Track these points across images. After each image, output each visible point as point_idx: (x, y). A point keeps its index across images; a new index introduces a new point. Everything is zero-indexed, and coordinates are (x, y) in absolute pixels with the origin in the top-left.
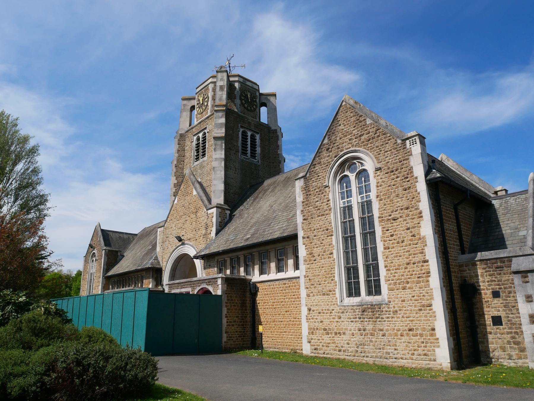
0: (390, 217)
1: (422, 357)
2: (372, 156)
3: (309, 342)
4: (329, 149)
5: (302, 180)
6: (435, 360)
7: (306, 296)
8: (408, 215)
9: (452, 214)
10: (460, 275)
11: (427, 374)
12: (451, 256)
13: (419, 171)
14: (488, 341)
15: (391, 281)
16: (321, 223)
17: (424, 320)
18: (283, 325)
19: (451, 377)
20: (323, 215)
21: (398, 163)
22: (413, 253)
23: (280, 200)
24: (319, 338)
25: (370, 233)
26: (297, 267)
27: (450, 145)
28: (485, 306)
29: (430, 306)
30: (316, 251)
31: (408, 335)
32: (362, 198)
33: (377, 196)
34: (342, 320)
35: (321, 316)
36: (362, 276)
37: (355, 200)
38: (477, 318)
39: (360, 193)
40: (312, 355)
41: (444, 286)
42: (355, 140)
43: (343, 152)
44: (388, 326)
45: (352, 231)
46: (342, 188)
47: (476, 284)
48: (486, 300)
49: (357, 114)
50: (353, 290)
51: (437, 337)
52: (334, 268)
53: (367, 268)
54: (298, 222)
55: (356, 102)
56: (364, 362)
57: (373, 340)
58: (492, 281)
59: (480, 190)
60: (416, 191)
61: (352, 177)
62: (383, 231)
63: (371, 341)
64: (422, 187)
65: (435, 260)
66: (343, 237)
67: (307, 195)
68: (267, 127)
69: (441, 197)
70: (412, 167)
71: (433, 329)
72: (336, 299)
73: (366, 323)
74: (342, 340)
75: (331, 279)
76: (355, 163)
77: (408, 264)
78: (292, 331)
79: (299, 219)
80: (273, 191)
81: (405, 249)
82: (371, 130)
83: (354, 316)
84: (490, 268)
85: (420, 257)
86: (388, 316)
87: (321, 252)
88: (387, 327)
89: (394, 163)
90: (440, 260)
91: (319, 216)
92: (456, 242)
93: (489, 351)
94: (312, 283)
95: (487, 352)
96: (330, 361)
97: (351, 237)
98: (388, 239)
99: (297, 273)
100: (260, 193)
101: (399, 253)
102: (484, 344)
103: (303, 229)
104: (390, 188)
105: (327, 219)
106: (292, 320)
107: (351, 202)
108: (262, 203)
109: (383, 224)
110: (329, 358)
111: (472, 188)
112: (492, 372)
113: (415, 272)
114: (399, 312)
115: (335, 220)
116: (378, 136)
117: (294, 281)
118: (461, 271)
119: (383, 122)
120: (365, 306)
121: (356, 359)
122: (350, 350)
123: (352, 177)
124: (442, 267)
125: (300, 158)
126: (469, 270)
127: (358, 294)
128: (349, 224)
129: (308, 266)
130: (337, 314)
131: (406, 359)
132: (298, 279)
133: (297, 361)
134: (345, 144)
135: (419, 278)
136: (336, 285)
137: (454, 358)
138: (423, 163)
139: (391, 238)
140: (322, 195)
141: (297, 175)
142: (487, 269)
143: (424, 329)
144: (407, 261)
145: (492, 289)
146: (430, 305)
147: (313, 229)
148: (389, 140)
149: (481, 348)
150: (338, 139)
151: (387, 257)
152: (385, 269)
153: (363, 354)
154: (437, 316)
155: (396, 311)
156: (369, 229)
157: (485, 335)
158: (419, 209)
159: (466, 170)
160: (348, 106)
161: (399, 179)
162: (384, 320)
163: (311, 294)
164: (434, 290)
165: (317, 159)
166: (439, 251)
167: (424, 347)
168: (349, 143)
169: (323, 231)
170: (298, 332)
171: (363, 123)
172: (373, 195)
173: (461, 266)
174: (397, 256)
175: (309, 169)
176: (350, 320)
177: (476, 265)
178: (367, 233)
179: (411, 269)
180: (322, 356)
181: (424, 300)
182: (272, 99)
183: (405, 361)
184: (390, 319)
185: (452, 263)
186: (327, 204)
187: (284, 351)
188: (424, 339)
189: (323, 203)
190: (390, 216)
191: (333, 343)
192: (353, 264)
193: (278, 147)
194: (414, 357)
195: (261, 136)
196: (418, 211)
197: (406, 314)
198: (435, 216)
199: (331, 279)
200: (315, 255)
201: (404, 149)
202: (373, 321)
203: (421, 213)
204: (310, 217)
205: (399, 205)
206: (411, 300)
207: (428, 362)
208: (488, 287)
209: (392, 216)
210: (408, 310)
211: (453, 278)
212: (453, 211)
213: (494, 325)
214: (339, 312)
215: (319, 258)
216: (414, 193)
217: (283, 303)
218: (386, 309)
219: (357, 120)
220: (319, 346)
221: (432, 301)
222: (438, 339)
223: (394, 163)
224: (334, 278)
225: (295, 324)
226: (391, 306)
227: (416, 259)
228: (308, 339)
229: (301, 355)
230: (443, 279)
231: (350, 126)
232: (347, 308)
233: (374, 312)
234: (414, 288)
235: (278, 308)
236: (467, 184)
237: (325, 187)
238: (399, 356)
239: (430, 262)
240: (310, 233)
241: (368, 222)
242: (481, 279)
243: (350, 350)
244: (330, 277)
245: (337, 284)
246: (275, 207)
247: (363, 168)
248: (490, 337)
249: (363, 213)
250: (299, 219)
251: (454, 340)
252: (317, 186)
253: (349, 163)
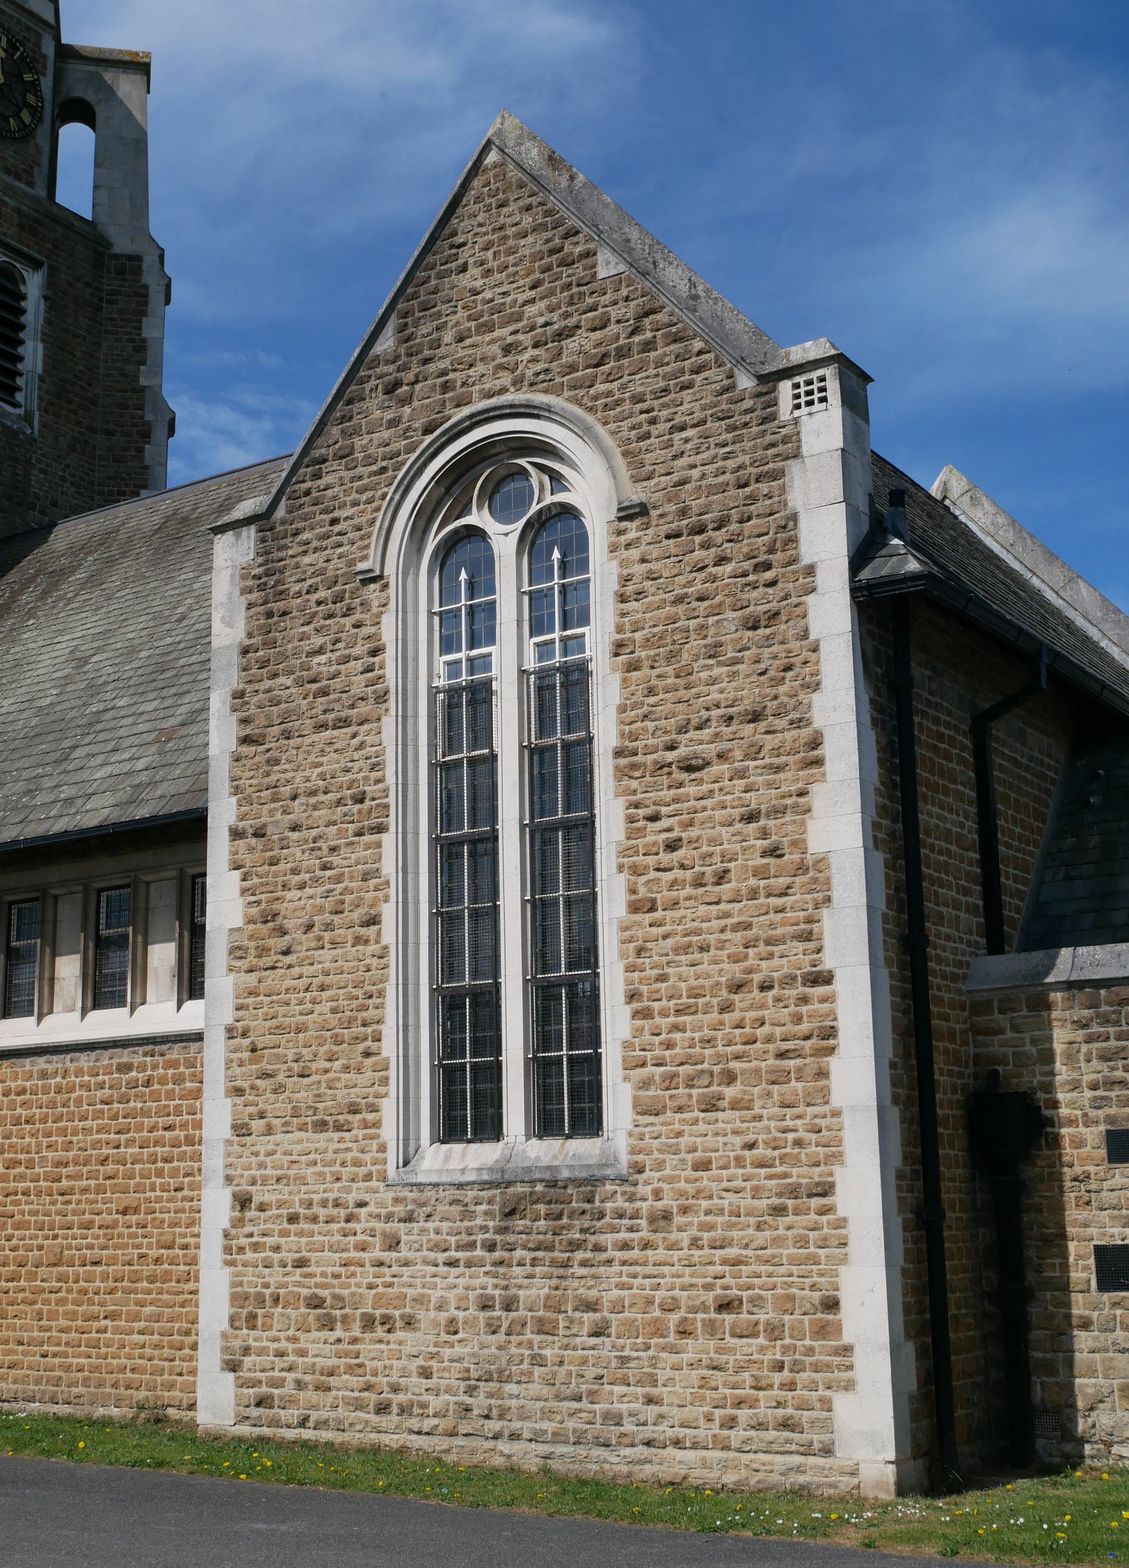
0: (670, 756)
1: (772, 1434)
2: (610, 442)
3: (233, 1367)
4: (397, 384)
5: (250, 534)
6: (827, 1451)
7: (227, 1133)
8: (754, 751)
9: (962, 761)
10: (972, 1050)
11: (789, 1517)
12: (939, 960)
13: (825, 536)
14: (1070, 1363)
15: (649, 1069)
16: (331, 763)
17: (794, 1261)
18: (105, 1277)
19: (891, 1528)
20: (344, 722)
21: (732, 492)
22: (763, 934)
23: (131, 633)
24: (283, 1345)
25: (568, 827)
26: (191, 982)
27: (1002, 430)
28: (1070, 1197)
29: (823, 1195)
30: (296, 905)
31: (711, 1328)
32: (544, 650)
33: (618, 648)
34: (404, 1253)
35: (301, 1234)
36: (512, 1041)
37: (510, 658)
38: (1031, 1253)
39: (538, 625)
40: (245, 1430)
41: (896, 1100)
42: (531, 353)
43: (466, 411)
44: (622, 1286)
45: (482, 813)
46: (448, 593)
47: (1041, 1096)
48: (1078, 1170)
49: (551, 221)
50: (466, 1109)
51: (847, 1338)
52: (381, 994)
53: (543, 998)
54: (214, 750)
55: (552, 160)
56: (498, 1461)
57: (547, 1352)
58: (1110, 1084)
59: (1103, 654)
60: (805, 635)
61: (504, 539)
62: (631, 820)
63: (538, 1361)
64: (831, 616)
65: (863, 974)
66: (434, 841)
67: (270, 615)
68: (84, 237)
69: (918, 672)
70: (794, 517)
71: (832, 1305)
72: (382, 1149)
73: (517, 1270)
74: (393, 1357)
75: (361, 1047)
76: (523, 473)
77: (737, 987)
78: (148, 1310)
79: (221, 735)
80: (94, 581)
81: (727, 915)
82: (614, 313)
83: (465, 1238)
84: (1106, 1021)
85: (797, 957)
86: (624, 1235)
87: (321, 910)
88: (616, 1293)
89: (712, 490)
90: (885, 973)
91: (323, 726)
92: (967, 892)
93: (1073, 1406)
94: (264, 1065)
95: (1063, 1409)
96: (329, 1463)
97: (474, 841)
98: (651, 860)
99: (193, 1015)
100: (25, 585)
101: (697, 932)
102: (1054, 1372)
103: (237, 790)
104: (681, 609)
105: (361, 746)
106: (154, 1253)
107: (488, 667)
108: (31, 639)
109: (634, 784)
110: (329, 1445)
111: (1063, 644)
112: (1077, 1503)
113: (766, 1028)
114: (678, 1220)
115: (402, 751)
116: (649, 346)
117: (175, 1052)
118: (978, 1031)
119: (674, 276)
120: (520, 1189)
121: (459, 1451)
122: (435, 1403)
123: (504, 539)
124: (895, 1007)
125: (267, 425)
126: (1015, 1028)
127: (490, 1127)
128: (473, 776)
129: (251, 979)
130: (379, 1226)
131: (695, 1446)
132: (194, 1046)
133: (160, 1464)
134: (480, 368)
135: (782, 1055)
136: (385, 1081)
137: (914, 1438)
138: (848, 498)
139: (665, 858)
140: (348, 621)
141: (227, 505)
142: (1095, 1029)
143: (787, 1304)
144: (735, 971)
145: (1110, 1120)
146: (826, 1190)
147: (286, 791)
148: (697, 371)
149: (1038, 1393)
150: (448, 337)
151: (639, 952)
152: (627, 1010)
153: (494, 1425)
154: (853, 1243)
155: (667, 1216)
156: (567, 809)
157: (1062, 1331)
158: (809, 723)
159: (1051, 556)
160: (514, 174)
161: (729, 568)
162: (604, 1256)
163: (257, 1125)
164: (847, 1119)
165: (335, 431)
166: (886, 932)
167: (782, 1386)
168: (502, 367)
169: (339, 802)
170: (178, 1318)
171: (580, 270)
172: (597, 637)
173: (979, 1007)
174: (686, 949)
175: (287, 482)
176: (441, 1257)
177: (1048, 1006)
178: (553, 828)
179: (751, 1015)
180: (290, 1434)
181: (796, 1161)
182: (125, 86)
183: (691, 1455)
184: (635, 1254)
185: (940, 990)
186: (369, 669)
187: (100, 1412)
188: (786, 1349)
189: (346, 660)
190: (671, 747)
191: (350, 1369)
192: (475, 975)
193: (140, 351)
194: (736, 1436)
195: (50, 283)
196: (805, 733)
197: (711, 1227)
198: (881, 762)
199: (361, 1047)
200: (289, 924)
201: (764, 420)
202: (554, 1263)
203: (815, 742)
204: (275, 730)
205: (715, 696)
206: (739, 1162)
207: (797, 1459)
208: (1093, 1113)
209: (682, 751)
210: (721, 1212)
211: (939, 1062)
212: (968, 743)
213: (1103, 1287)
214: (389, 1218)
215: (306, 941)
216: (794, 645)
217: (110, 1168)
218: (620, 1203)
219: (552, 252)
220: (279, 1383)
221: (837, 1170)
222: (847, 1350)
223: (712, 490)
224: (374, 1046)
225: (166, 1277)
226: (644, 1190)
227: (776, 968)
228: (225, 1350)
229: (188, 1435)
230: (893, 1065)
231: (513, 278)
232: (430, 1194)
233: (559, 1217)
234: (758, 1103)
235: (85, 1190)
236: (1044, 623)
237: (365, 582)
238: (665, 1431)
239: (838, 985)
240: (272, 813)
241: (561, 774)
242: (1062, 1072)
243: (435, 1403)
244: (357, 1039)
245: (392, 1073)
246: (102, 664)
247: (560, 497)
248: (1083, 1340)
249: (544, 725)
250: (221, 735)
251: (921, 1354)
252: (321, 572)
253: (493, 469)
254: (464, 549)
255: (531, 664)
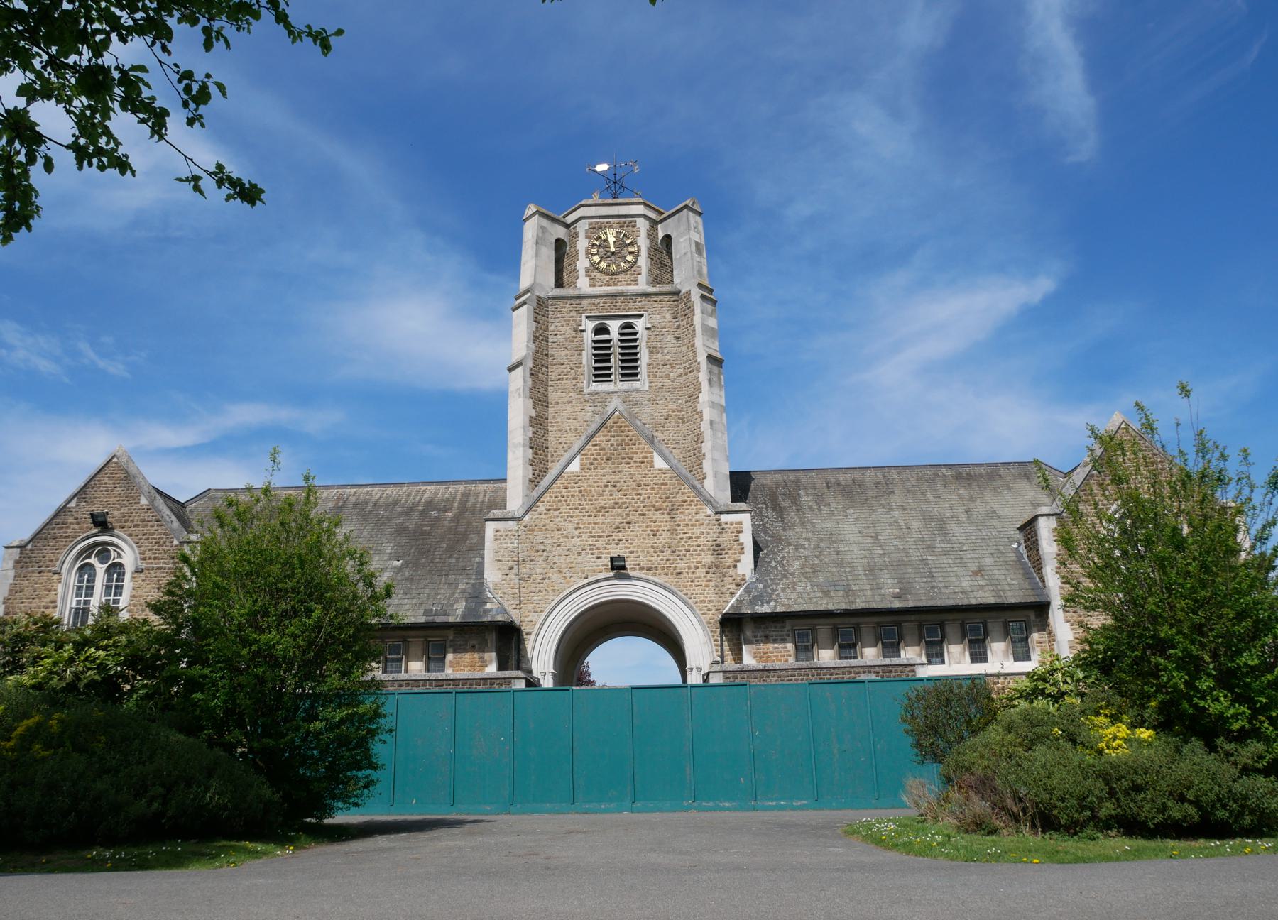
61: (101, 569)
123: (101, 569)
254: (86, 569)
255: (74, 605)
